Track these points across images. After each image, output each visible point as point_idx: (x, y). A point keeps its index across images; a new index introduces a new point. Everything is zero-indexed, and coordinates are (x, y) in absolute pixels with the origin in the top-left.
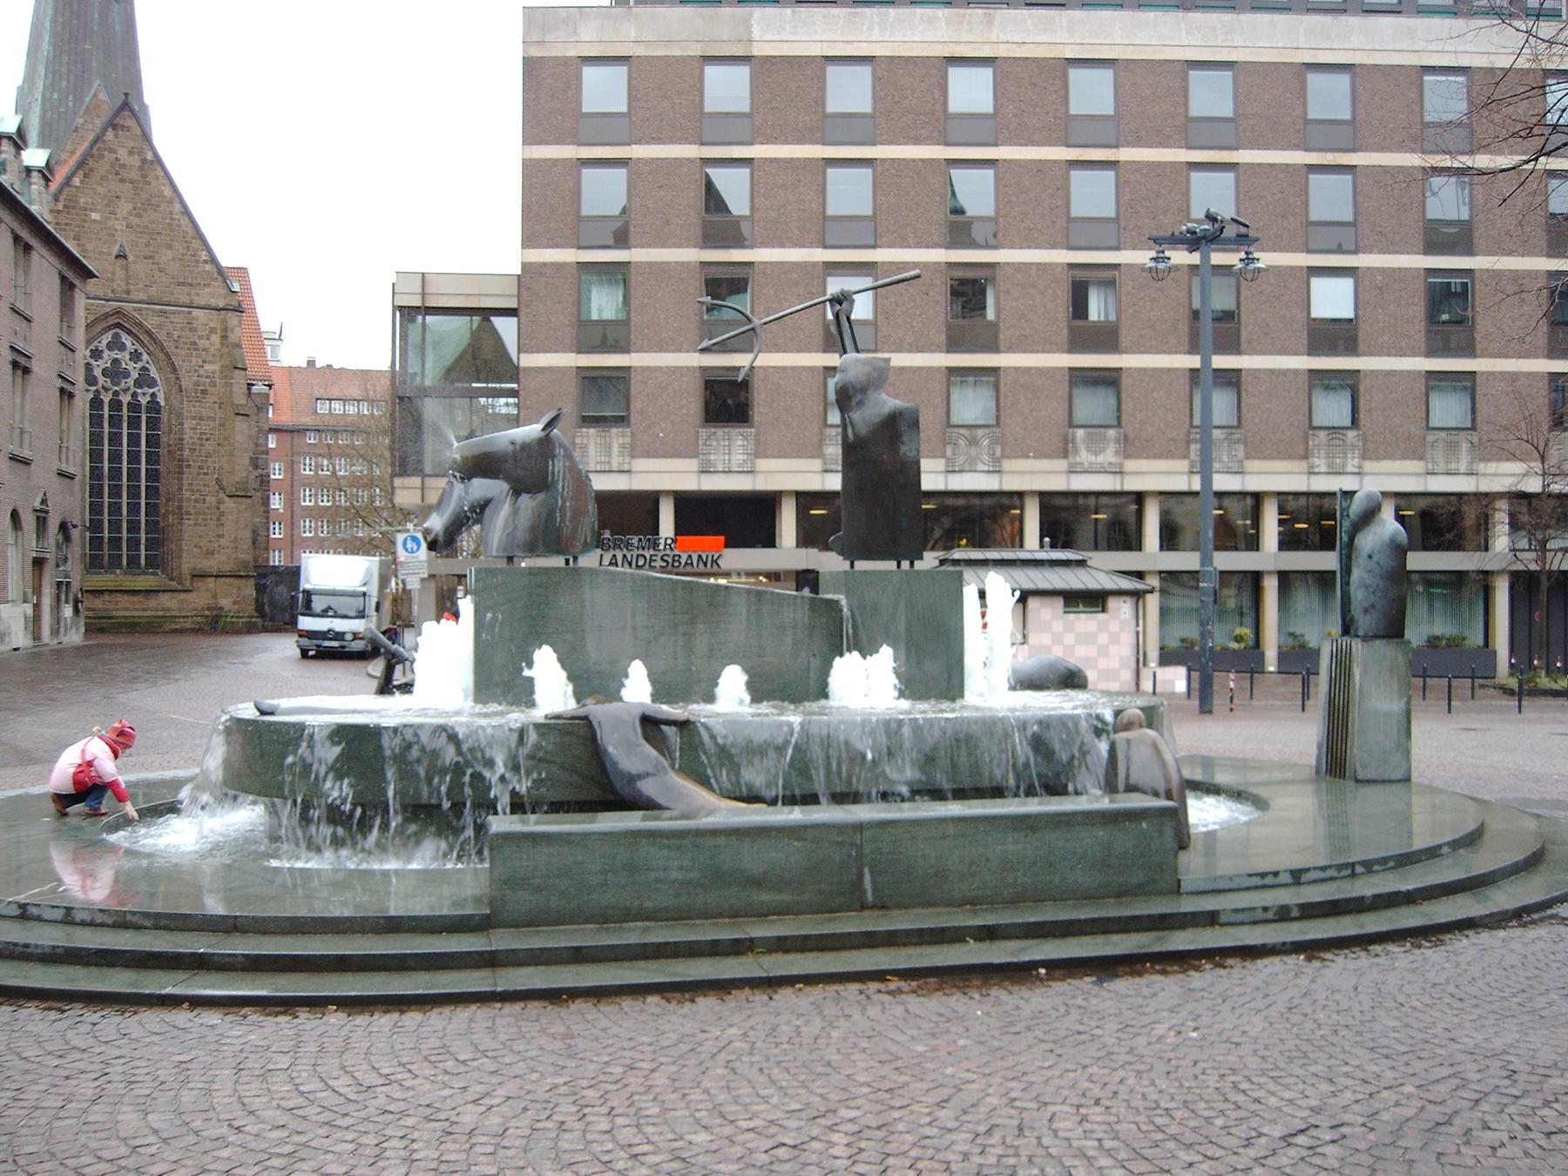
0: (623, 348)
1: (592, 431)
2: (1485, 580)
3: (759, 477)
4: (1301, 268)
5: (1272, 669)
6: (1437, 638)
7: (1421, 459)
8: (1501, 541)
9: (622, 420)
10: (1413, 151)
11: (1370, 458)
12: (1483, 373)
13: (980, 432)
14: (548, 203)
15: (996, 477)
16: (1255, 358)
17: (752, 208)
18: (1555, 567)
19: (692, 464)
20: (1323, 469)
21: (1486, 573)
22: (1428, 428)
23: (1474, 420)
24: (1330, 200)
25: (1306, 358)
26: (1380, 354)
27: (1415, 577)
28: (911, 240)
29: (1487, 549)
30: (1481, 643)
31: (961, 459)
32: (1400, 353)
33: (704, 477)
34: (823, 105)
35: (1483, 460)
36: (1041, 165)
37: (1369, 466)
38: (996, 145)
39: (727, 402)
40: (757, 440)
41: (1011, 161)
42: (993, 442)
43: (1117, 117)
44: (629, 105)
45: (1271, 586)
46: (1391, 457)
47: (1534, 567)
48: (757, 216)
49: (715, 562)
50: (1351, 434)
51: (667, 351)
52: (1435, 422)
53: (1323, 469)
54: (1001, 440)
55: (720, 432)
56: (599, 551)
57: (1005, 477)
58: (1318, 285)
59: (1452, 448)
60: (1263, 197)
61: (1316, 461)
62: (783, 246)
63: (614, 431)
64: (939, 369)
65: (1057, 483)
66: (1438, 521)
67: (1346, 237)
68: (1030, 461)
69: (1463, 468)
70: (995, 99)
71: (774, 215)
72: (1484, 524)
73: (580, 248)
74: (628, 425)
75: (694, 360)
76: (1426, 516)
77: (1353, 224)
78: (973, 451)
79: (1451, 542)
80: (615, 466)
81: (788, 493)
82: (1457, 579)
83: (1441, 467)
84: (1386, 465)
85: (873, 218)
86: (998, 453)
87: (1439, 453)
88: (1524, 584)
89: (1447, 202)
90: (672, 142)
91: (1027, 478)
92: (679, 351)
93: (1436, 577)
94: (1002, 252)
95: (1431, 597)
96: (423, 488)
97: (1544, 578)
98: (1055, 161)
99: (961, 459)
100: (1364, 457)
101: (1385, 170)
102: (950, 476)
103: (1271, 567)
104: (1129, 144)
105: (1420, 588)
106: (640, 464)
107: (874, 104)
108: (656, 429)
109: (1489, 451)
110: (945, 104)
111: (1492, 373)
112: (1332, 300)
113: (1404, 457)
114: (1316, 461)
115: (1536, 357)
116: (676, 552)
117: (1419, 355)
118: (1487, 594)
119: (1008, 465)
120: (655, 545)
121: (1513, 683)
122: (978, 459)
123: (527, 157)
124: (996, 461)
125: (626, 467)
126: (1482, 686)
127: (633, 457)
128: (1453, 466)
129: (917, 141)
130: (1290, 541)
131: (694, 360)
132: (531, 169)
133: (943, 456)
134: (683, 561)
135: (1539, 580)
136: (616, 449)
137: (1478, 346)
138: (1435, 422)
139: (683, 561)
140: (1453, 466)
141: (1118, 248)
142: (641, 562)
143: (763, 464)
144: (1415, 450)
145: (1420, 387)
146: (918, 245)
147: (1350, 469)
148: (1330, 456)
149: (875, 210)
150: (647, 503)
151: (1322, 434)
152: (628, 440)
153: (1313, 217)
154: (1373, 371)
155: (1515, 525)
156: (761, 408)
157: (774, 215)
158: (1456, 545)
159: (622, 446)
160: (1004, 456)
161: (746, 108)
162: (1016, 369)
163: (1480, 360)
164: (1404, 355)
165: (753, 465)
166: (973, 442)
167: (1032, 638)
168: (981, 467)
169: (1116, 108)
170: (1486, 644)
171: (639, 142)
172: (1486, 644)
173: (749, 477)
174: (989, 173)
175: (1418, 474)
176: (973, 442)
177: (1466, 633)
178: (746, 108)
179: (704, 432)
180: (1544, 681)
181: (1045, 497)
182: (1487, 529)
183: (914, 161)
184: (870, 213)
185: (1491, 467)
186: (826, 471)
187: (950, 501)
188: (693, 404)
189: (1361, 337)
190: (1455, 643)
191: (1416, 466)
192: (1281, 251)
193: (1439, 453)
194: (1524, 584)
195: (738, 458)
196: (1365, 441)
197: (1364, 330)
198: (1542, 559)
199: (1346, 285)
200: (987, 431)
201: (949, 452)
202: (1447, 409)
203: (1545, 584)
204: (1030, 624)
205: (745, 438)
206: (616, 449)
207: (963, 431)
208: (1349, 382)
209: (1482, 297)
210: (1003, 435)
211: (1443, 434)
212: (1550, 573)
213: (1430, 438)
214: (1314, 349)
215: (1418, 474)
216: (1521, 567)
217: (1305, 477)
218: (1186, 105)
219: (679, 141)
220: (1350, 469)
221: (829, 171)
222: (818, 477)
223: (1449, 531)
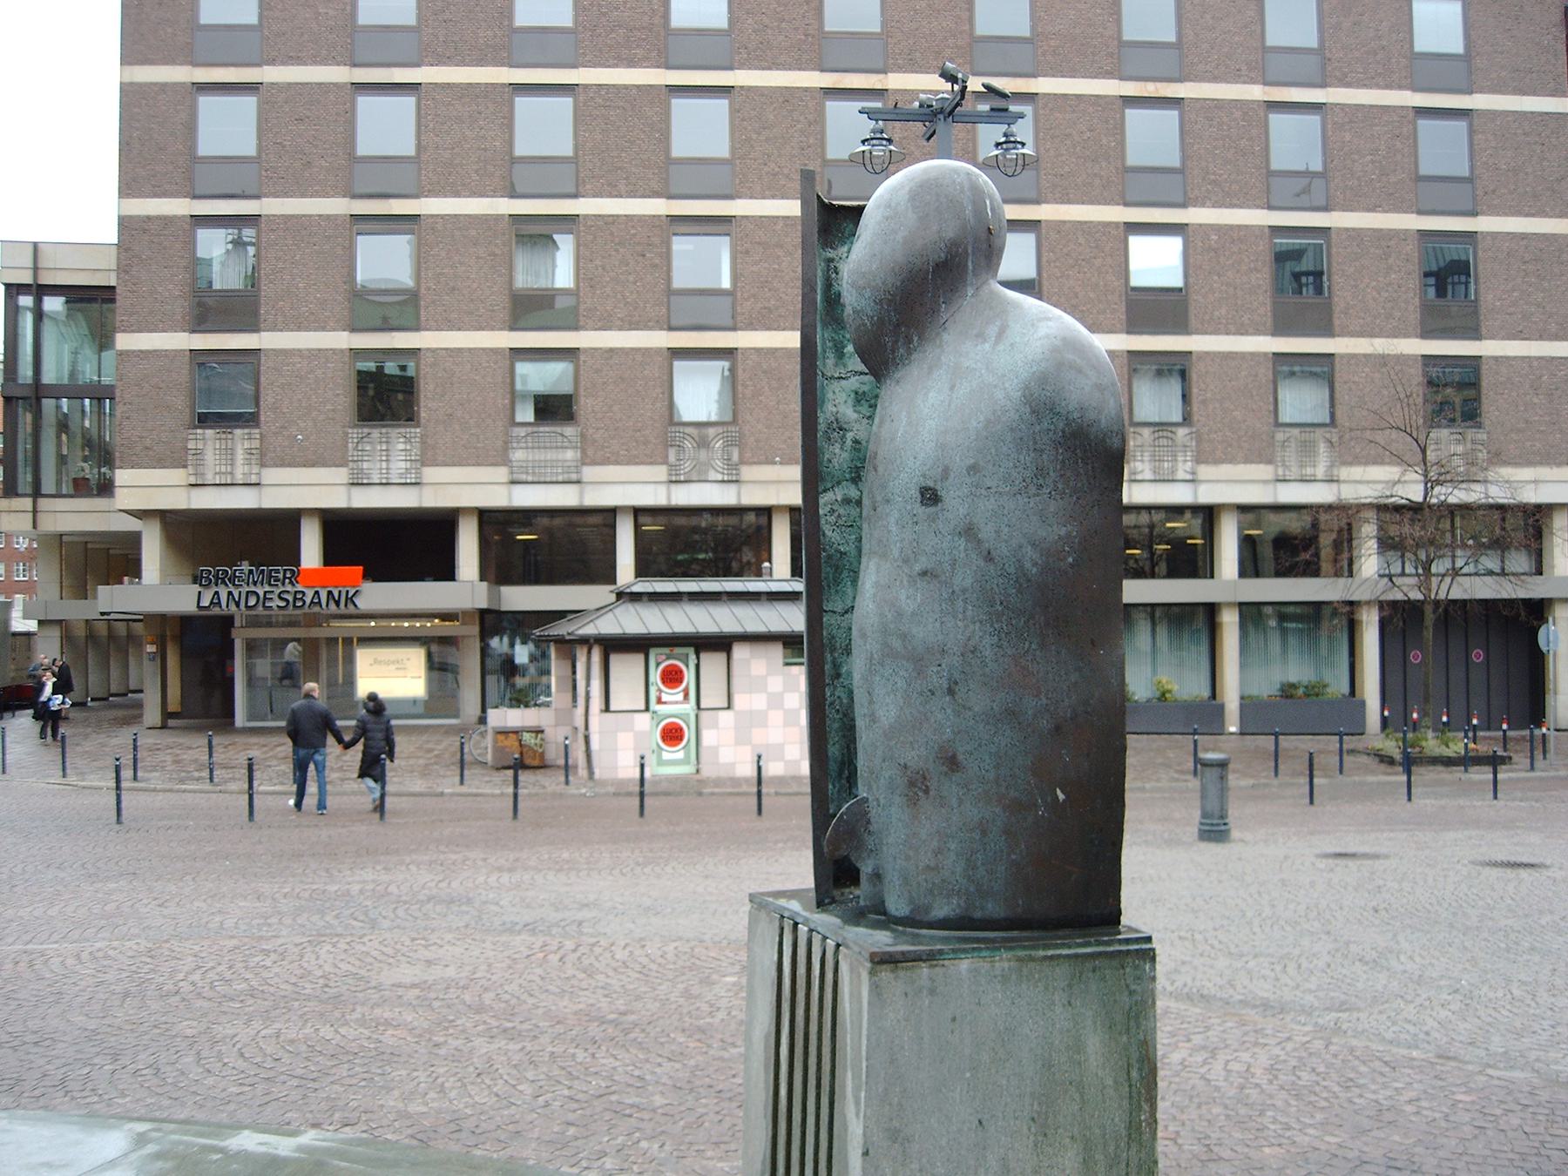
0: (251, 324)
1: (210, 432)
2: (1348, 613)
3: (427, 491)
4: (1117, 224)
5: (1233, 729)
6: (1293, 686)
7: (1269, 462)
8: (1370, 563)
9: (250, 420)
10: (1253, 81)
11: (1206, 462)
12: (1342, 356)
13: (711, 431)
14: (153, 141)
15: (733, 488)
16: (1207, 338)
17: (419, 146)
18: (1442, 596)
19: (341, 475)
20: (1148, 475)
21: (1351, 603)
22: (1278, 424)
23: (1332, 415)
24: (1151, 139)
25: (1124, 336)
26: (1216, 332)
27: (1269, 610)
28: (622, 187)
29: (1351, 575)
30: (1346, 689)
31: (688, 465)
32: (1242, 331)
33: (356, 491)
34: (511, 17)
35: (1345, 463)
36: (788, 94)
37: (1205, 471)
38: (731, 68)
39: (385, 396)
40: (423, 442)
41: (750, 88)
42: (728, 445)
43: (1467, 57)
44: (261, 16)
45: (1230, 621)
46: (1231, 460)
47: (1416, 595)
48: (424, 157)
49: (350, 600)
50: (1182, 432)
51: (307, 329)
52: (1285, 417)
53: (1148, 475)
54: (740, 442)
55: (376, 433)
56: (197, 588)
57: (745, 489)
58: (683, 246)
59: (1307, 450)
60: (1069, 135)
61: (1139, 466)
62: (457, 194)
63: (238, 432)
64: (658, 351)
65: (498, 498)
66: (1289, 544)
67: (1318, 192)
68: (777, 467)
69: (1320, 472)
70: (730, 11)
71: (447, 154)
72: (1345, 541)
73: (195, 197)
74: (257, 425)
75: (342, 340)
76: (673, 534)
77: (1469, 180)
78: (703, 454)
79: (1308, 563)
80: (239, 478)
81: (780, 508)
82: (1314, 612)
83: (1294, 472)
84: (1226, 470)
85: (574, 160)
86: (735, 457)
87: (1291, 455)
88: (1401, 621)
89: (1442, 150)
90: (315, 63)
91: (619, 489)
92: (323, 329)
93: (1291, 609)
94: (739, 202)
95: (1284, 632)
96: (35, 511)
97: (1428, 610)
98: (806, 89)
99: (688, 465)
100: (1199, 460)
101: (1219, 104)
102: (674, 487)
103: (1231, 599)
104: (900, 69)
105: (1273, 623)
106: (272, 475)
107: (576, 16)
108: (293, 430)
109: (1347, 454)
110: (666, 16)
111: (1354, 356)
112: (1156, 262)
113: (1247, 460)
114: (1139, 466)
115: (1406, 336)
116: (299, 588)
117: (1265, 334)
118: (1353, 628)
119: (748, 472)
120: (295, 577)
121: (1391, 747)
122: (709, 465)
123: (127, 80)
124: (732, 467)
125: (254, 479)
126: (1352, 752)
127: (263, 465)
128: (1309, 471)
129: (631, 63)
130: (1251, 565)
131: (342, 340)
132: (131, 96)
133: (665, 462)
134: (308, 600)
135: (1422, 613)
136: (240, 455)
137: (1336, 322)
138: (1285, 417)
139: (308, 600)
140: (1309, 471)
141: (575, 196)
142: (252, 602)
143: (431, 474)
144: (1261, 453)
145: (1265, 373)
146: (632, 194)
147: (1181, 475)
148: (1156, 459)
149: (576, 148)
150: (284, 524)
151: (1146, 432)
152: (256, 444)
153: (1423, 171)
154: (1207, 353)
155: (1387, 544)
156: (429, 402)
157: (447, 154)
158: (1311, 570)
159: (249, 452)
160: (742, 462)
161: (411, 21)
162: (758, 350)
163: (1338, 340)
164: (1246, 333)
165: (418, 473)
166: (703, 443)
167: (738, 700)
168: (713, 475)
169: (884, 24)
170: (1214, 696)
171: (272, 62)
172: (1214, 696)
173: (413, 491)
174: (567, 102)
175: (1265, 482)
176: (703, 443)
177: (1328, 678)
178: (411, 21)
179: (354, 433)
180: (1431, 744)
181: (486, 517)
182: (1350, 548)
183: (626, 87)
184: (571, 154)
185: (1356, 472)
186: (513, 482)
187: (681, 521)
188: (343, 398)
189: (1192, 312)
190: (1314, 691)
191: (1263, 471)
192: (1091, 202)
193: (1291, 455)
194: (1401, 621)
195: (399, 466)
196: (1199, 440)
197: (1196, 300)
198: (1424, 585)
199: (1174, 244)
200: (720, 430)
201: (672, 458)
202: (1300, 402)
203: (1430, 617)
204: (735, 681)
205: (408, 440)
206: (240, 455)
207: (689, 430)
208: (1176, 367)
209: (1484, 266)
210: (742, 435)
211: (1296, 431)
212: (1437, 603)
213: (1280, 436)
214: (1133, 327)
215: (1265, 482)
216: (1399, 596)
217: (343, 489)
218: (971, 20)
219: (324, 61)
220: (1181, 475)
221: (674, 102)
222: (503, 490)
223: (1306, 549)
